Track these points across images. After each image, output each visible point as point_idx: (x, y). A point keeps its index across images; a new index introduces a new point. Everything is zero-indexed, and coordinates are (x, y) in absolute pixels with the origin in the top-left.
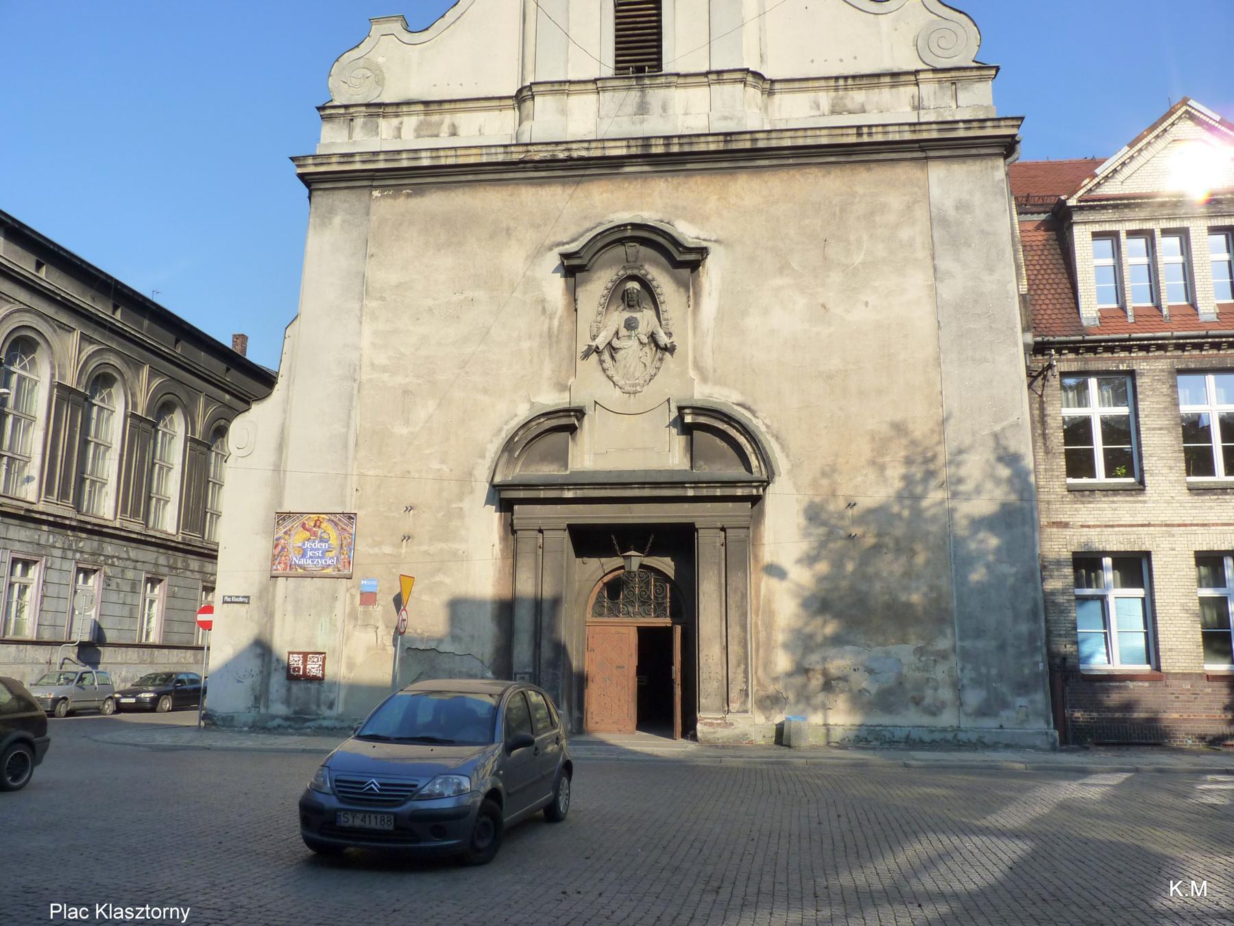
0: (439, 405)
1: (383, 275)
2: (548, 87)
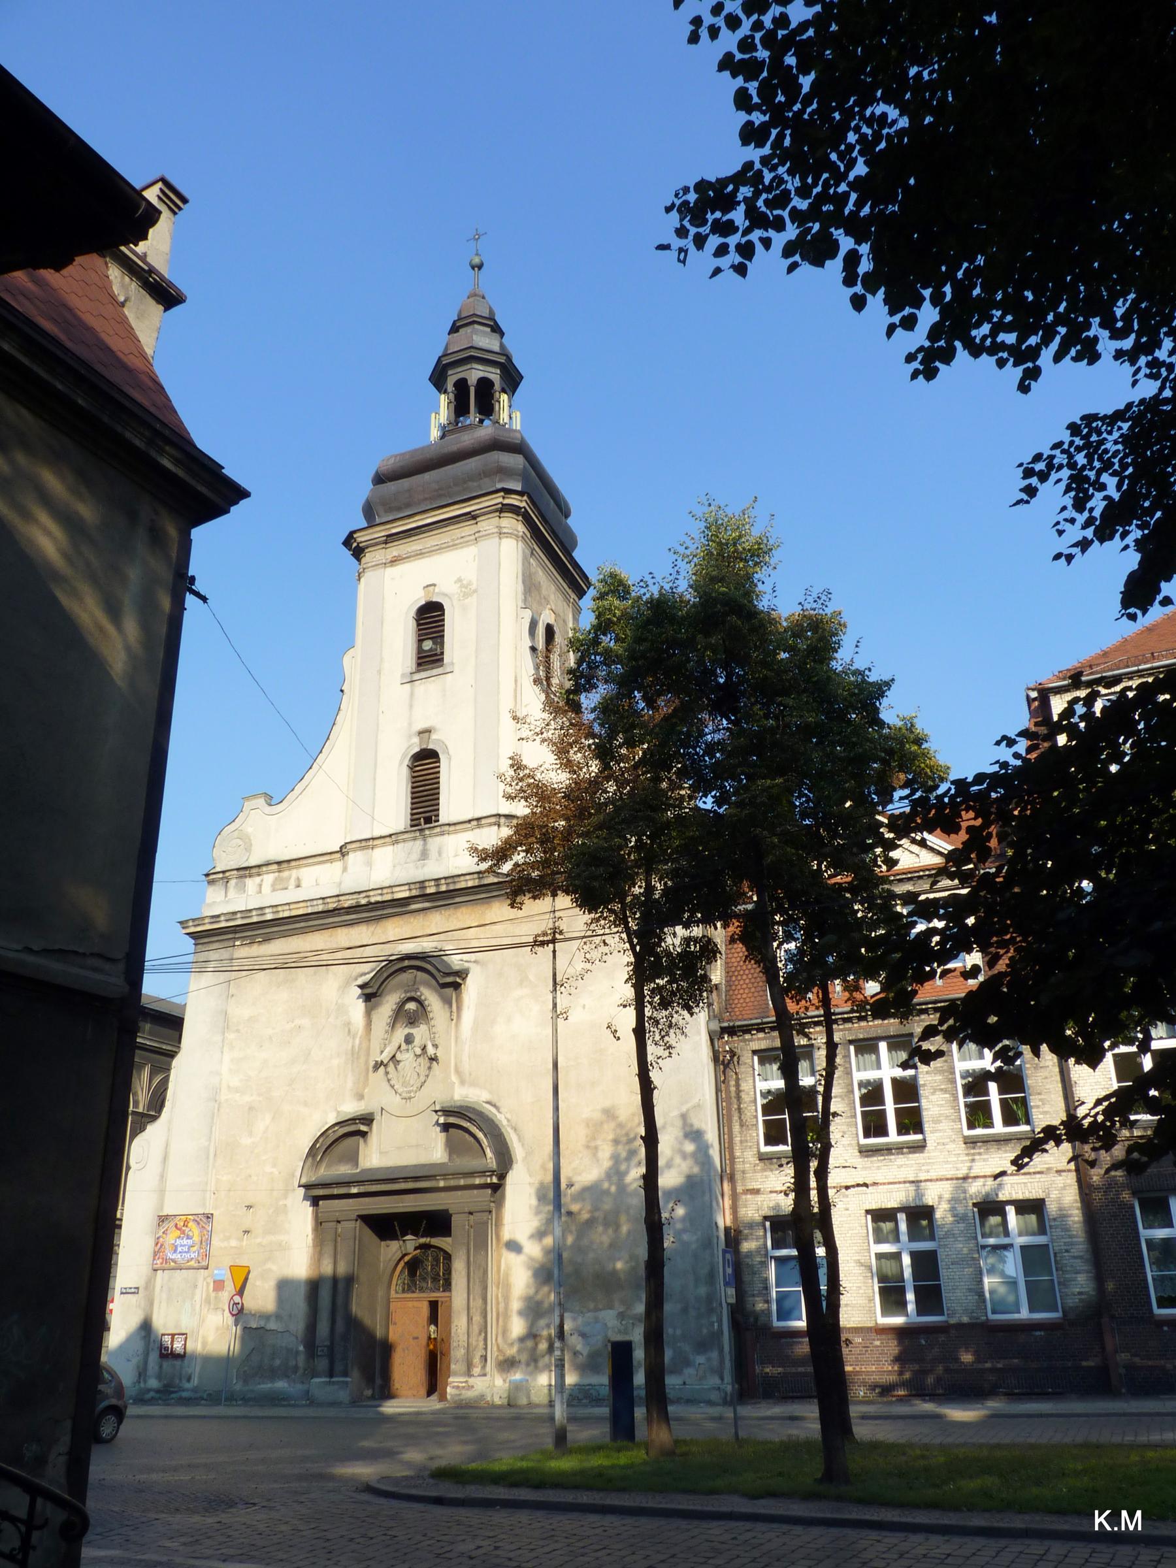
0: (273, 1118)
1: (240, 1011)
2: (358, 845)
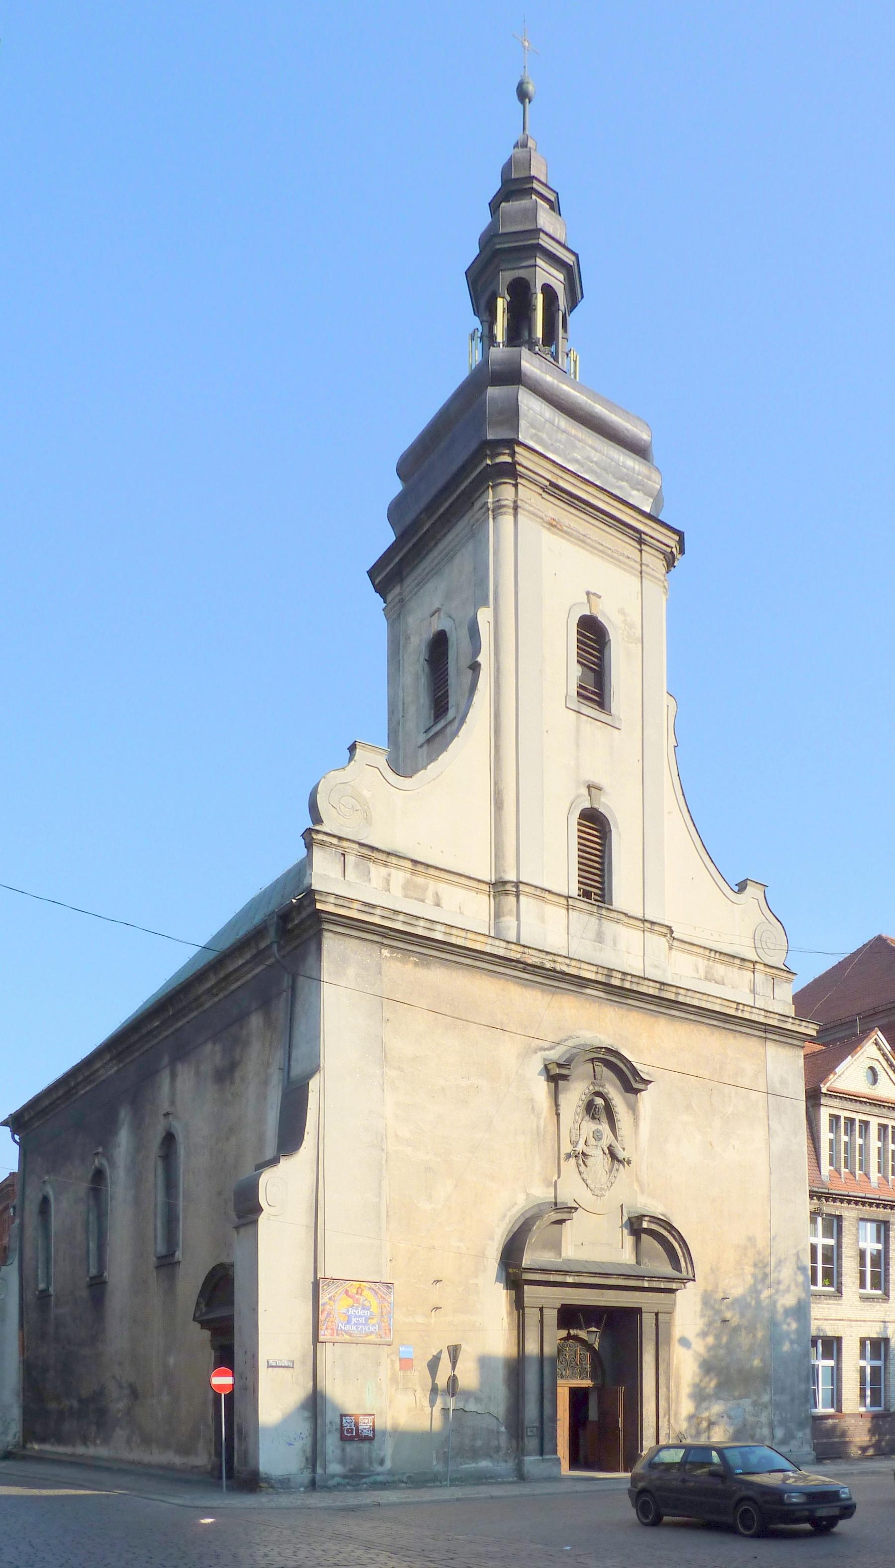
0: (456, 1186)
